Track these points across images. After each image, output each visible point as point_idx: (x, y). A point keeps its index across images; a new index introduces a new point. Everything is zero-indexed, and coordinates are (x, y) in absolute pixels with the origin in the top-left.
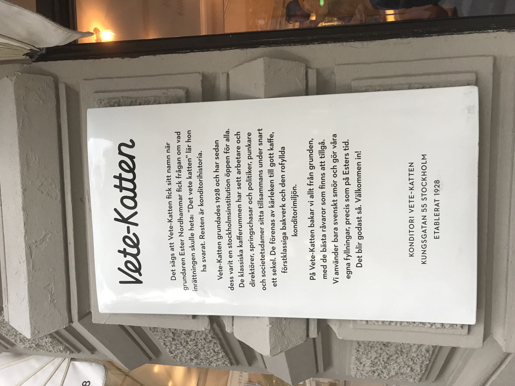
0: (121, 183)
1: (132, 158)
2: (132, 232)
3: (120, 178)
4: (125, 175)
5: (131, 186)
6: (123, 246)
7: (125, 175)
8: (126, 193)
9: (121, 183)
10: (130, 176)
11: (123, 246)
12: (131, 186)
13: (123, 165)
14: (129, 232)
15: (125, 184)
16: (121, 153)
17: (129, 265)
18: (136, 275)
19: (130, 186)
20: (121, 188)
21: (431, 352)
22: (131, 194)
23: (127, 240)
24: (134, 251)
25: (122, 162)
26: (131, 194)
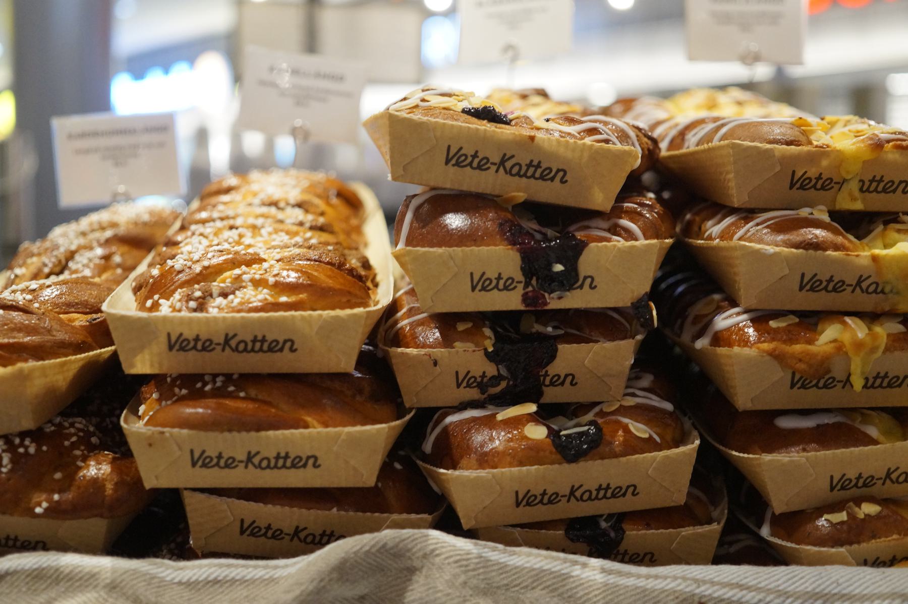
0: (533, 166)
1: (552, 179)
2: (518, 285)
3: (538, 166)
4: (539, 171)
5: (529, 174)
6: (481, 155)
7: (539, 171)
8: (524, 168)
9: (533, 166)
10: (537, 175)
11: (481, 155)
12: (529, 174)
13: (547, 171)
14: (517, 282)
15: (532, 170)
16: (558, 171)
17: (488, 282)
18: (479, 287)
19: (529, 174)
20: (529, 165)
21: (237, 271)
22: (522, 173)
23: (510, 281)
24: (475, 164)
25: (551, 170)
26: (522, 173)
